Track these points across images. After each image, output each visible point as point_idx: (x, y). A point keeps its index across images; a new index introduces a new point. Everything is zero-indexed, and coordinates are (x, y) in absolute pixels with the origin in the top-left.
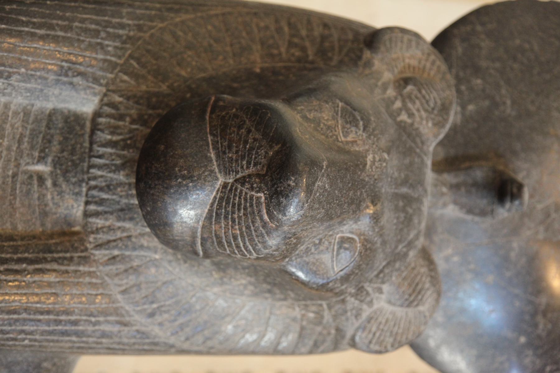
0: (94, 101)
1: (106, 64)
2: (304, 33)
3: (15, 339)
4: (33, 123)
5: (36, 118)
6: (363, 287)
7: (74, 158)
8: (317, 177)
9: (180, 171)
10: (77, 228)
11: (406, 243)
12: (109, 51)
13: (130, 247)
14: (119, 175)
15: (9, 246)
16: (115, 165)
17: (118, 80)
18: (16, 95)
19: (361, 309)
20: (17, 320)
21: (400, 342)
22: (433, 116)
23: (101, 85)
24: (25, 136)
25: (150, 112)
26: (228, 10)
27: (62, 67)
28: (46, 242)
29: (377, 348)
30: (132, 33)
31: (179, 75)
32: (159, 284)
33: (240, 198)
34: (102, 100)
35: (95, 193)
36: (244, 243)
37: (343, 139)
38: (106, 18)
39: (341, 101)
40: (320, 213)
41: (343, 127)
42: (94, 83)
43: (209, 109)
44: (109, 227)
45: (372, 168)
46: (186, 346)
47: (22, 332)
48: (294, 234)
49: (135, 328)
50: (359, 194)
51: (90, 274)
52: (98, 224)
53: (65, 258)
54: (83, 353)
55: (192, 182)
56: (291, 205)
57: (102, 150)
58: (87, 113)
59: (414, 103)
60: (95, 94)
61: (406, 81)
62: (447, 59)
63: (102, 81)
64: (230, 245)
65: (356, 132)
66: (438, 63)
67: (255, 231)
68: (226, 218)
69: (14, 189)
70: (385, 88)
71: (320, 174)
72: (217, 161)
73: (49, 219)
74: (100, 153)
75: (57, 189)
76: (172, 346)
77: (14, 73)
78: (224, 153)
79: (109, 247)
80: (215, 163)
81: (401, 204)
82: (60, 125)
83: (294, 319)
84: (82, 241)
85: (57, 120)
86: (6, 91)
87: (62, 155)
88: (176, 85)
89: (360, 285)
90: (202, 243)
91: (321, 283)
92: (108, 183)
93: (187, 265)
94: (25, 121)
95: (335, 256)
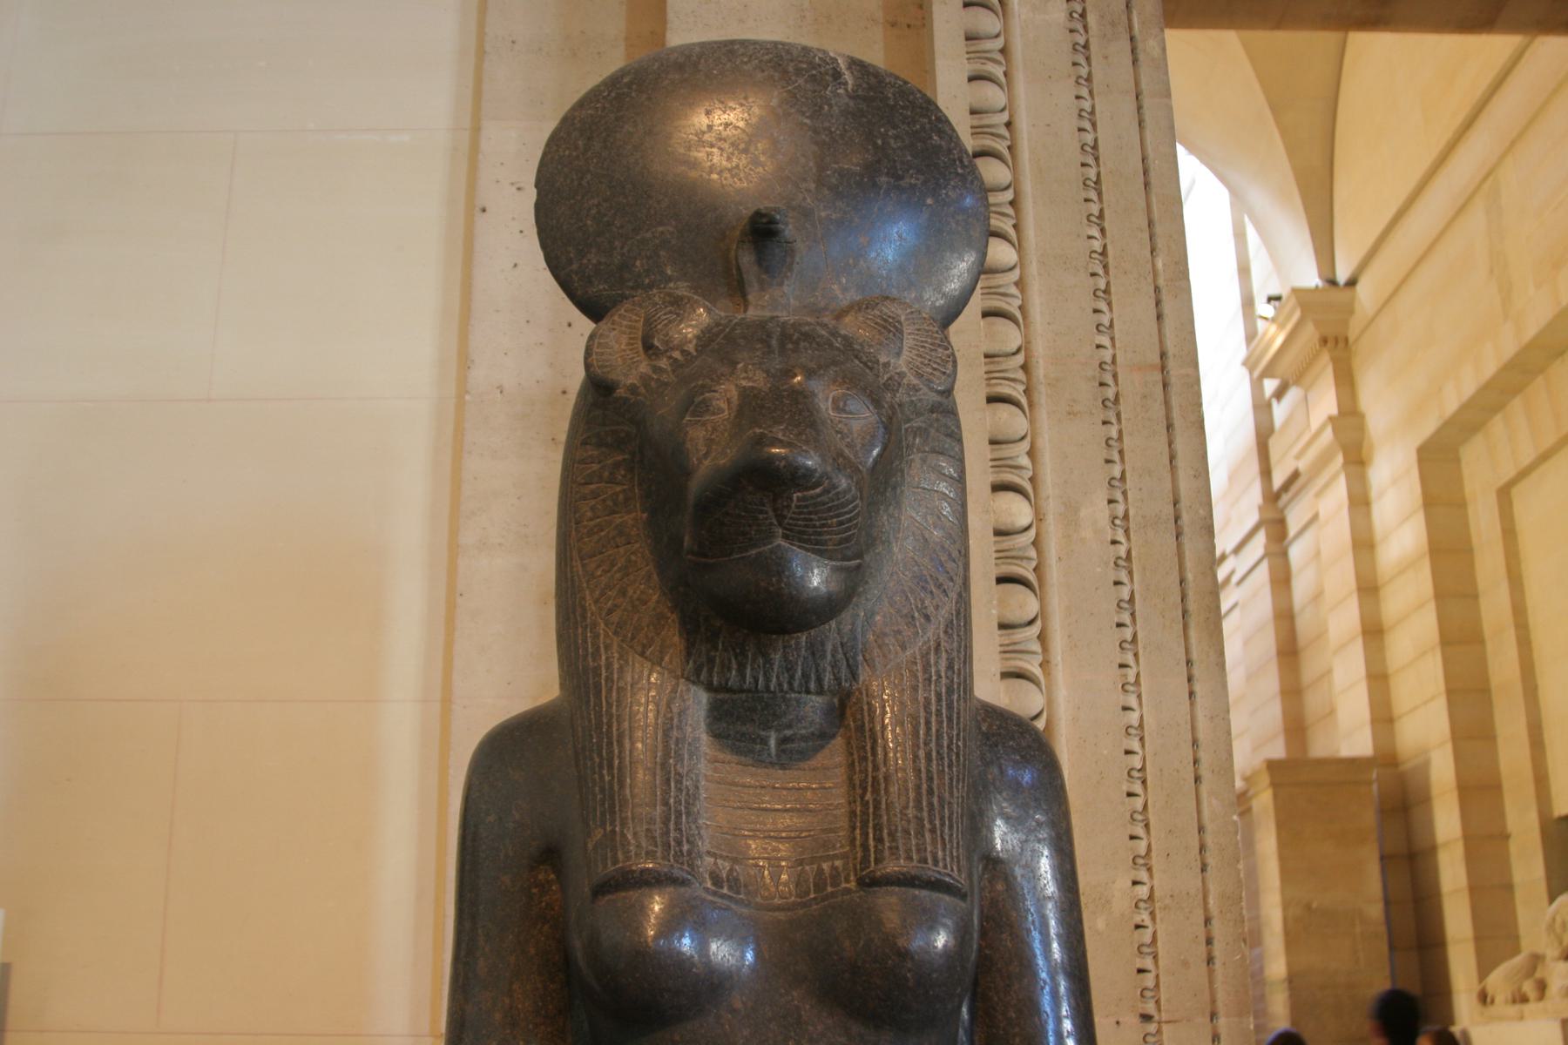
2: (595, 467)
3: (958, 755)
6: (884, 384)
7: (759, 708)
10: (836, 701)
11: (832, 338)
15: (860, 766)
17: (670, 666)
19: (908, 385)
20: (938, 752)
21: (942, 341)
23: (677, 684)
25: (703, 629)
26: (575, 554)
28: (853, 730)
29: (950, 366)
30: (616, 655)
31: (658, 602)
33: (798, 520)
35: (796, 684)
36: (846, 513)
37: (726, 413)
38: (603, 682)
39: (684, 417)
41: (714, 414)
43: (703, 560)
44: (832, 667)
45: (756, 381)
46: (959, 581)
47: (949, 747)
48: (834, 459)
49: (942, 635)
54: (972, 689)
56: (804, 464)
57: (748, 679)
58: (708, 700)
60: (688, 690)
62: (616, 302)
64: (849, 529)
66: (622, 311)
67: (833, 501)
68: (820, 534)
70: (657, 369)
71: (770, 435)
74: (751, 680)
76: (960, 595)
78: (751, 539)
80: (762, 549)
81: (790, 346)
82: (725, 725)
83: (924, 461)
85: (719, 729)
89: (882, 387)
91: (883, 430)
92: (785, 671)
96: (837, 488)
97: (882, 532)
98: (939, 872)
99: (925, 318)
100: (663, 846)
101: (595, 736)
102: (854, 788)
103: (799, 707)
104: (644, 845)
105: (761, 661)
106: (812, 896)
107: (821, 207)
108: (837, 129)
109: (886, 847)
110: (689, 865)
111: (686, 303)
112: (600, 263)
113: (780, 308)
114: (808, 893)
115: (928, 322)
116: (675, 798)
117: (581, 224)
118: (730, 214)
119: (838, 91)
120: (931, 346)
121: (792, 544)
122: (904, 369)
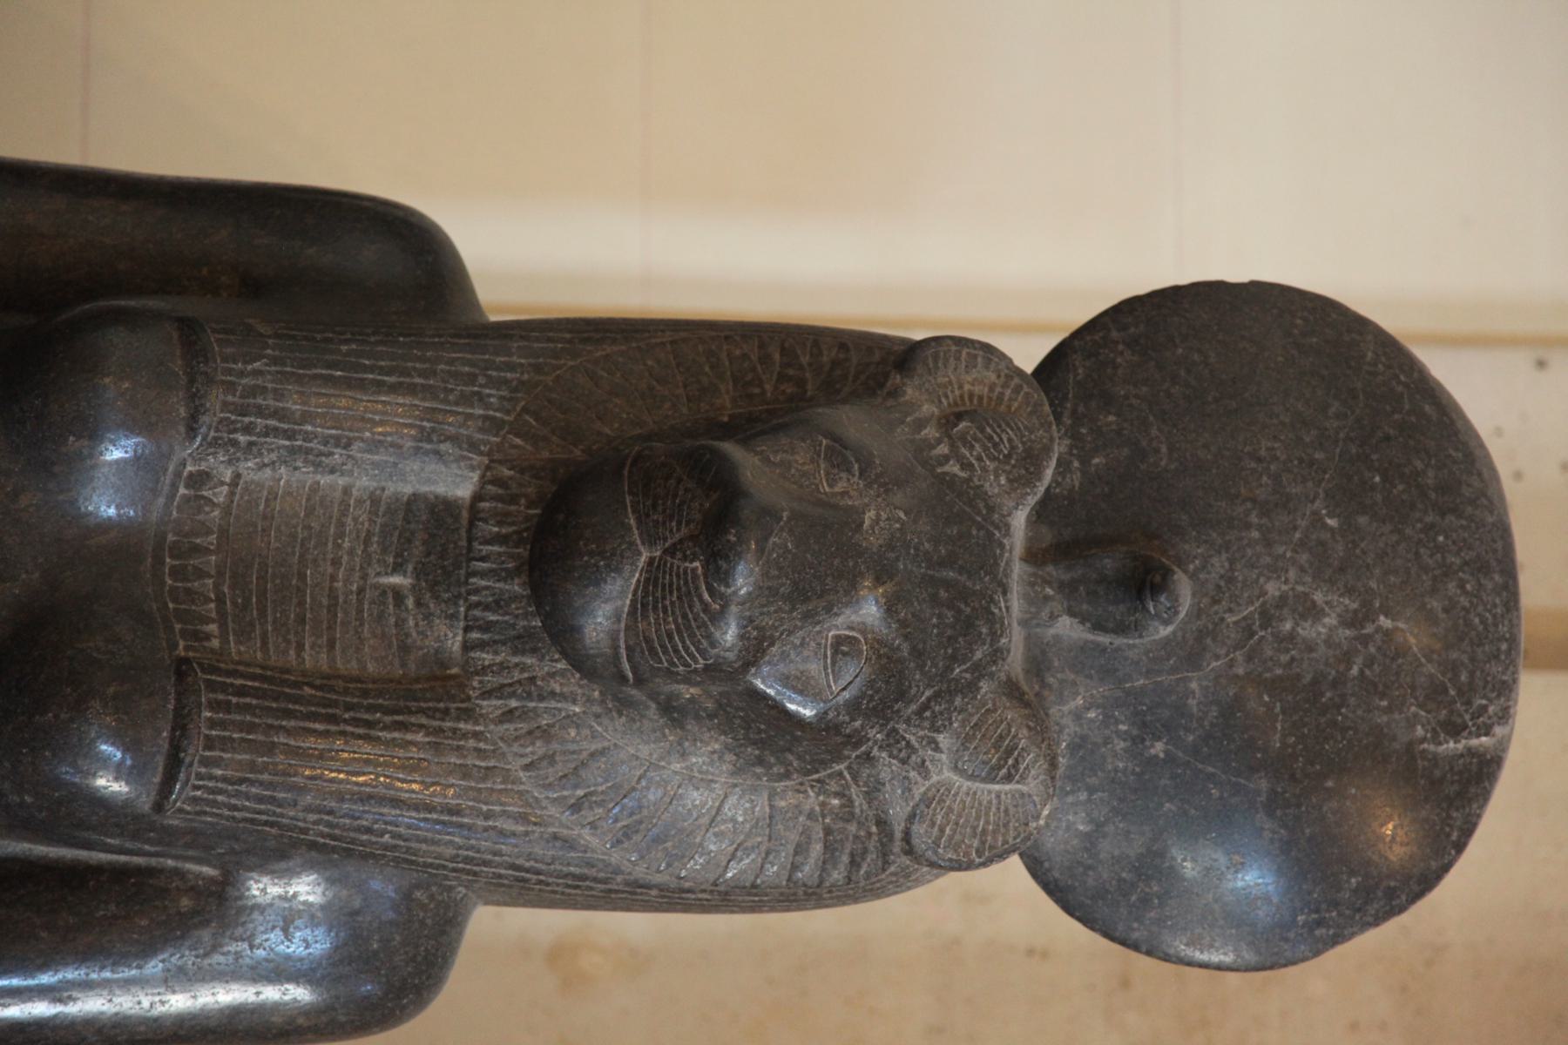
0: (472, 478)
1: (487, 423)
4: (383, 516)
5: (389, 508)
8: (772, 531)
9: (586, 545)
10: (455, 671)
12: (492, 403)
13: (535, 694)
14: (513, 584)
15: (354, 689)
16: (506, 570)
17: (507, 445)
18: (359, 474)
22: (1008, 468)
23: (481, 453)
24: (374, 535)
27: (422, 429)
30: (526, 377)
31: (599, 433)
32: (585, 755)
33: (671, 575)
34: (483, 477)
35: (477, 613)
38: (487, 357)
39: (826, 438)
40: (784, 585)
41: (827, 474)
42: (470, 452)
44: (501, 663)
45: (873, 529)
49: (551, 830)
50: (851, 564)
51: (477, 735)
52: (484, 659)
53: (436, 710)
55: (604, 558)
58: (463, 499)
59: (972, 447)
60: (472, 468)
61: (959, 417)
63: (482, 448)
64: (665, 652)
65: (849, 480)
67: (695, 620)
68: (655, 608)
69: (360, 611)
70: (920, 424)
72: (638, 529)
73: (412, 658)
74: (484, 553)
75: (423, 610)
77: (356, 439)
78: (648, 515)
79: (502, 694)
80: (636, 532)
82: (424, 518)
84: (462, 687)
85: (419, 510)
86: (344, 467)
87: (428, 560)
88: (594, 447)
90: (628, 655)
93: (623, 719)
94: (374, 512)
95: (829, 666)
96: (713, 624)
97: (695, 740)
98: (191, 765)
99: (1027, 824)
100: (242, 405)
101: (408, 339)
102: (323, 678)
103: (446, 618)
104: (244, 381)
105: (510, 566)
106: (171, 605)
107: (1205, 683)
108: (1345, 717)
109: (230, 697)
110: (215, 439)
111: (1027, 469)
112: (1116, 367)
113: (1033, 610)
114: (175, 601)
115: (1021, 829)
116: (312, 433)
117: (1177, 341)
118: (1187, 547)
119: (1419, 727)
120: (980, 829)
121: (642, 571)
122: (935, 778)
